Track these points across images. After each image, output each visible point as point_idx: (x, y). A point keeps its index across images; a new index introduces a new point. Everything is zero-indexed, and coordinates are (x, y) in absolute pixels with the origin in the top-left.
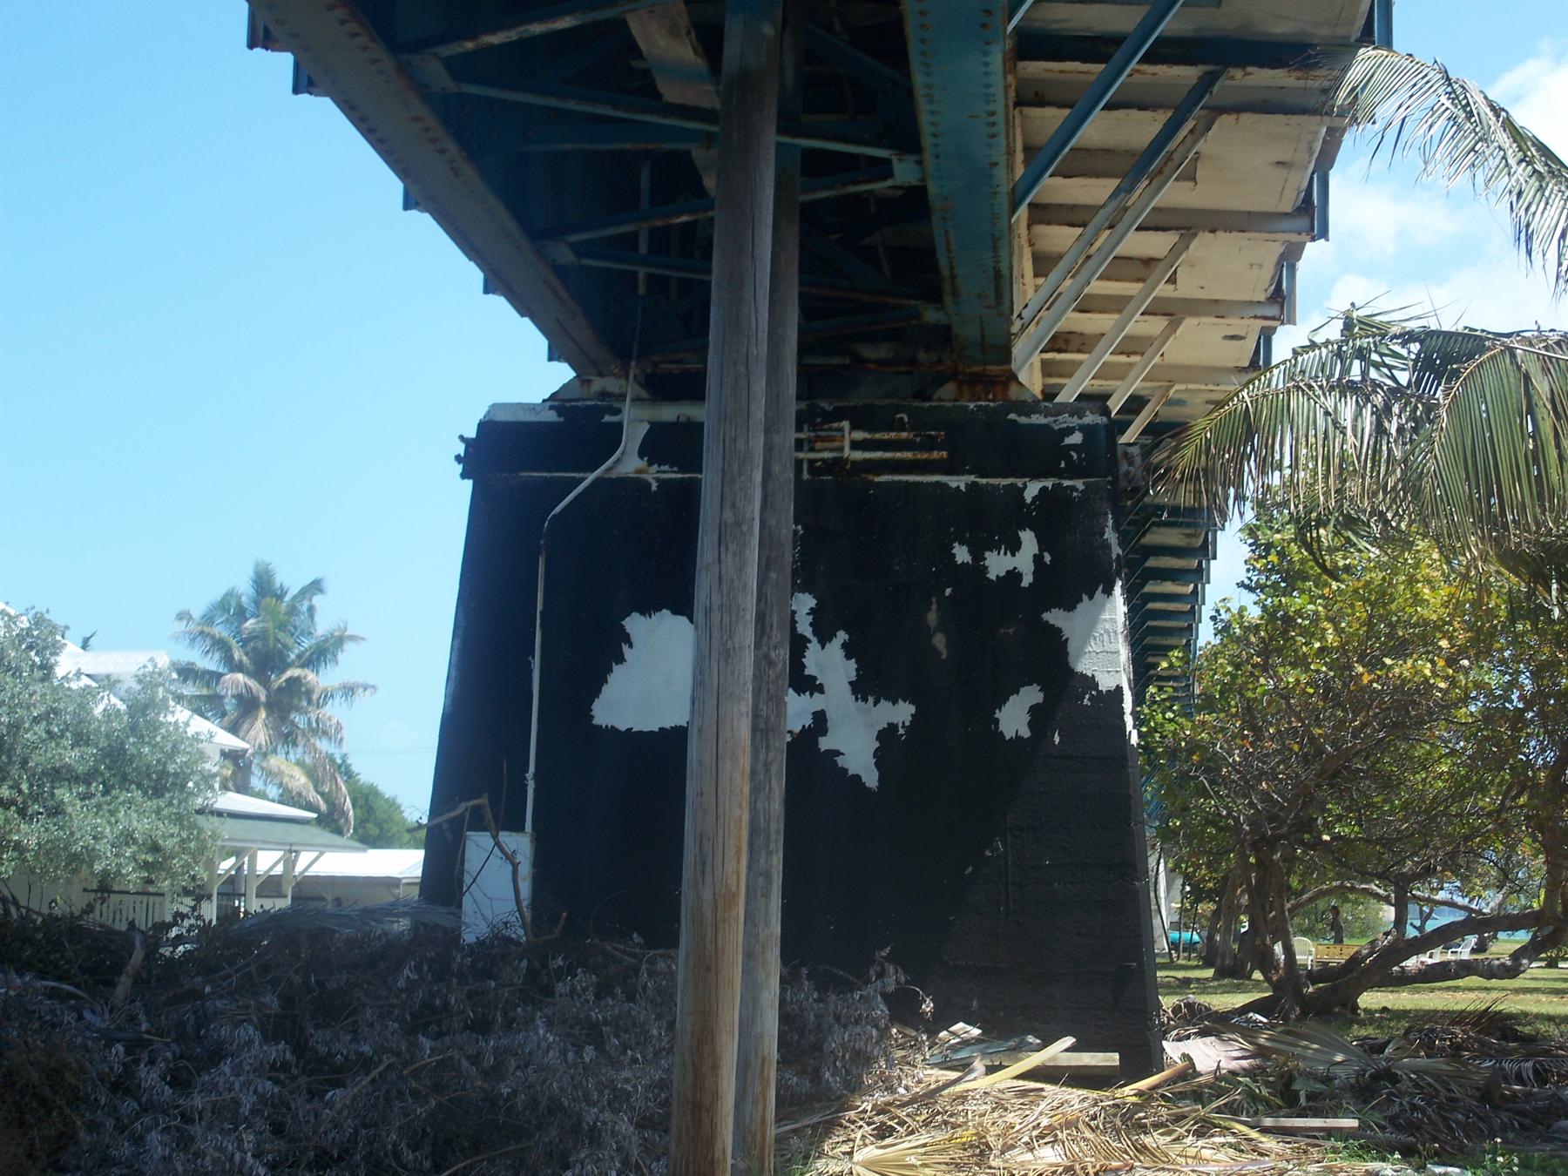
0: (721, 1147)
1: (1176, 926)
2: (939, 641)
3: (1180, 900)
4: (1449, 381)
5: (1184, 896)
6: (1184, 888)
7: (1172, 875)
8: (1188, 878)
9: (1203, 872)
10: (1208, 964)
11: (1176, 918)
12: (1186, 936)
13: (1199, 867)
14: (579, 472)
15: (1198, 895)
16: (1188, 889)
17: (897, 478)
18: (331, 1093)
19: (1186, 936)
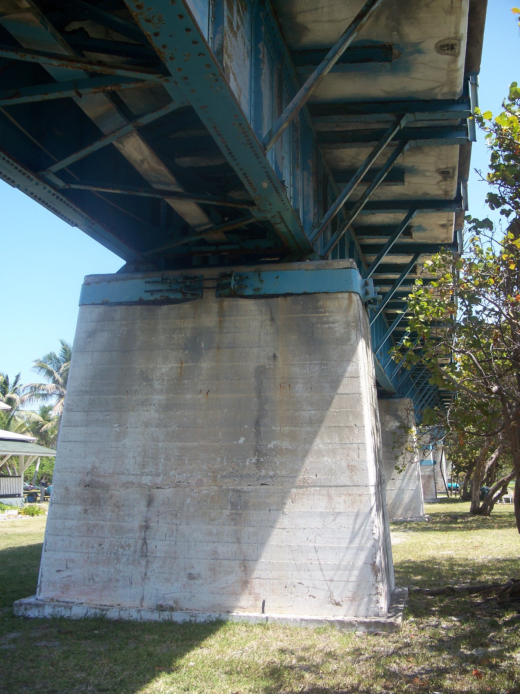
0: (385, 585)
1: (450, 481)
2: (109, 88)
3: (451, 471)
4: (326, 652)
5: (453, 470)
6: (453, 467)
7: (448, 461)
8: (454, 462)
9: (461, 459)
10: (465, 498)
11: (450, 478)
12: (454, 484)
13: (459, 457)
14: (223, 10)
15: (458, 468)
16: (454, 467)
17: (16, 123)
18: (492, 634)
19: (454, 484)
